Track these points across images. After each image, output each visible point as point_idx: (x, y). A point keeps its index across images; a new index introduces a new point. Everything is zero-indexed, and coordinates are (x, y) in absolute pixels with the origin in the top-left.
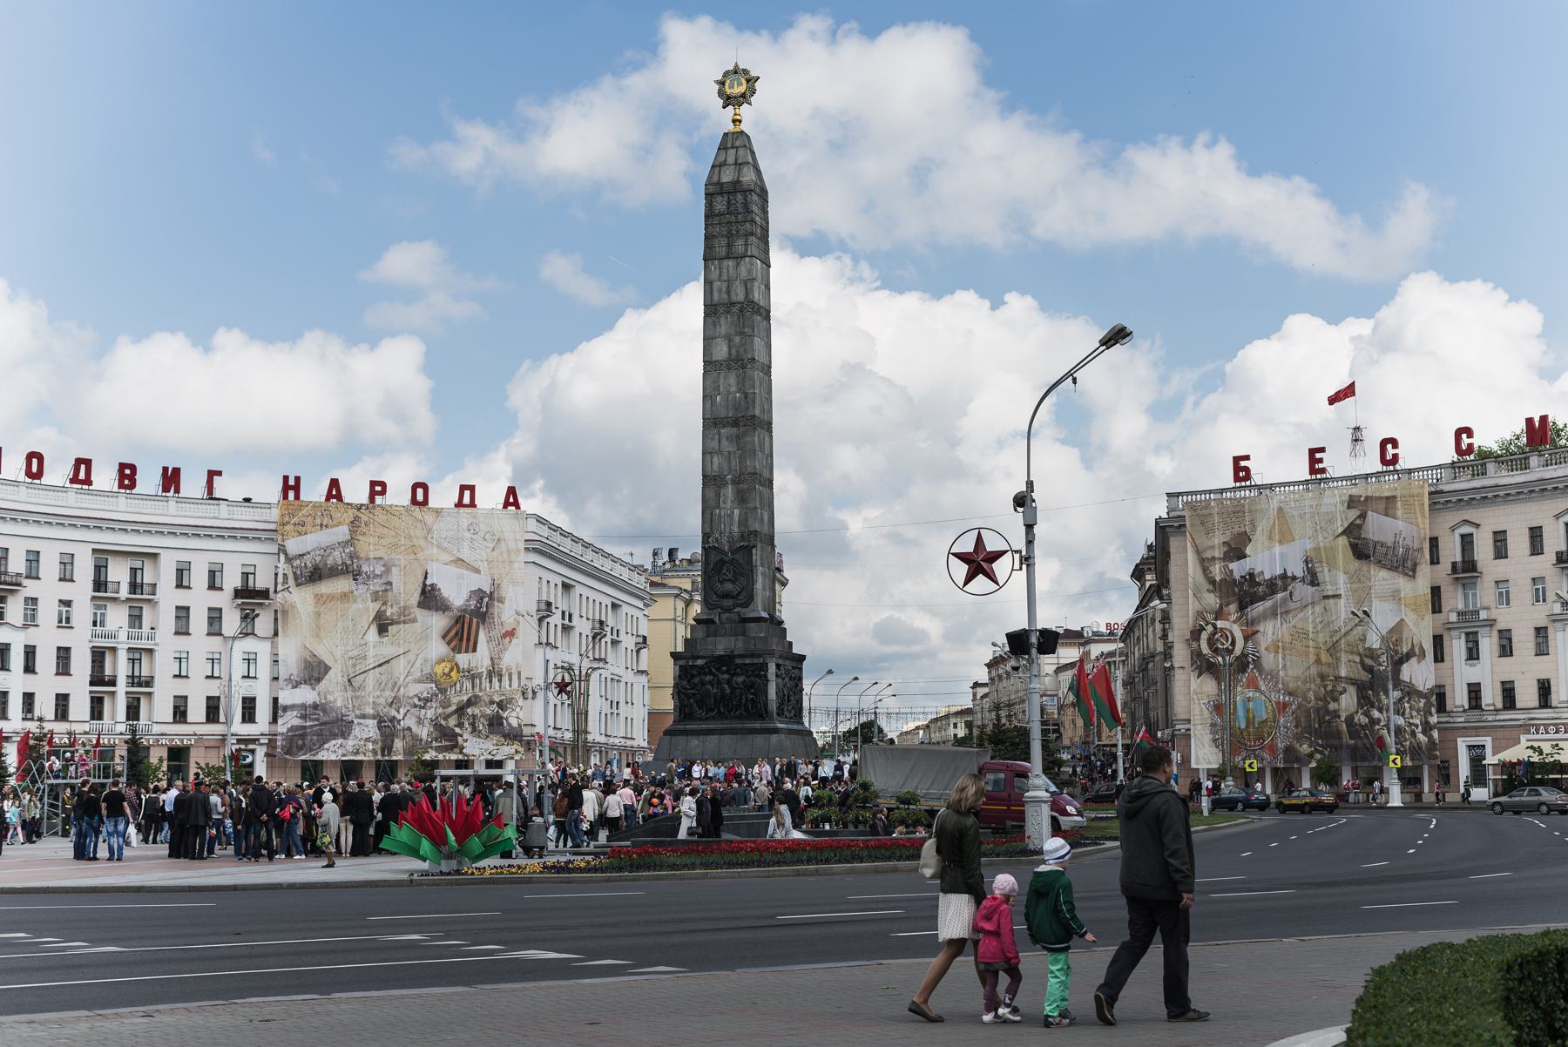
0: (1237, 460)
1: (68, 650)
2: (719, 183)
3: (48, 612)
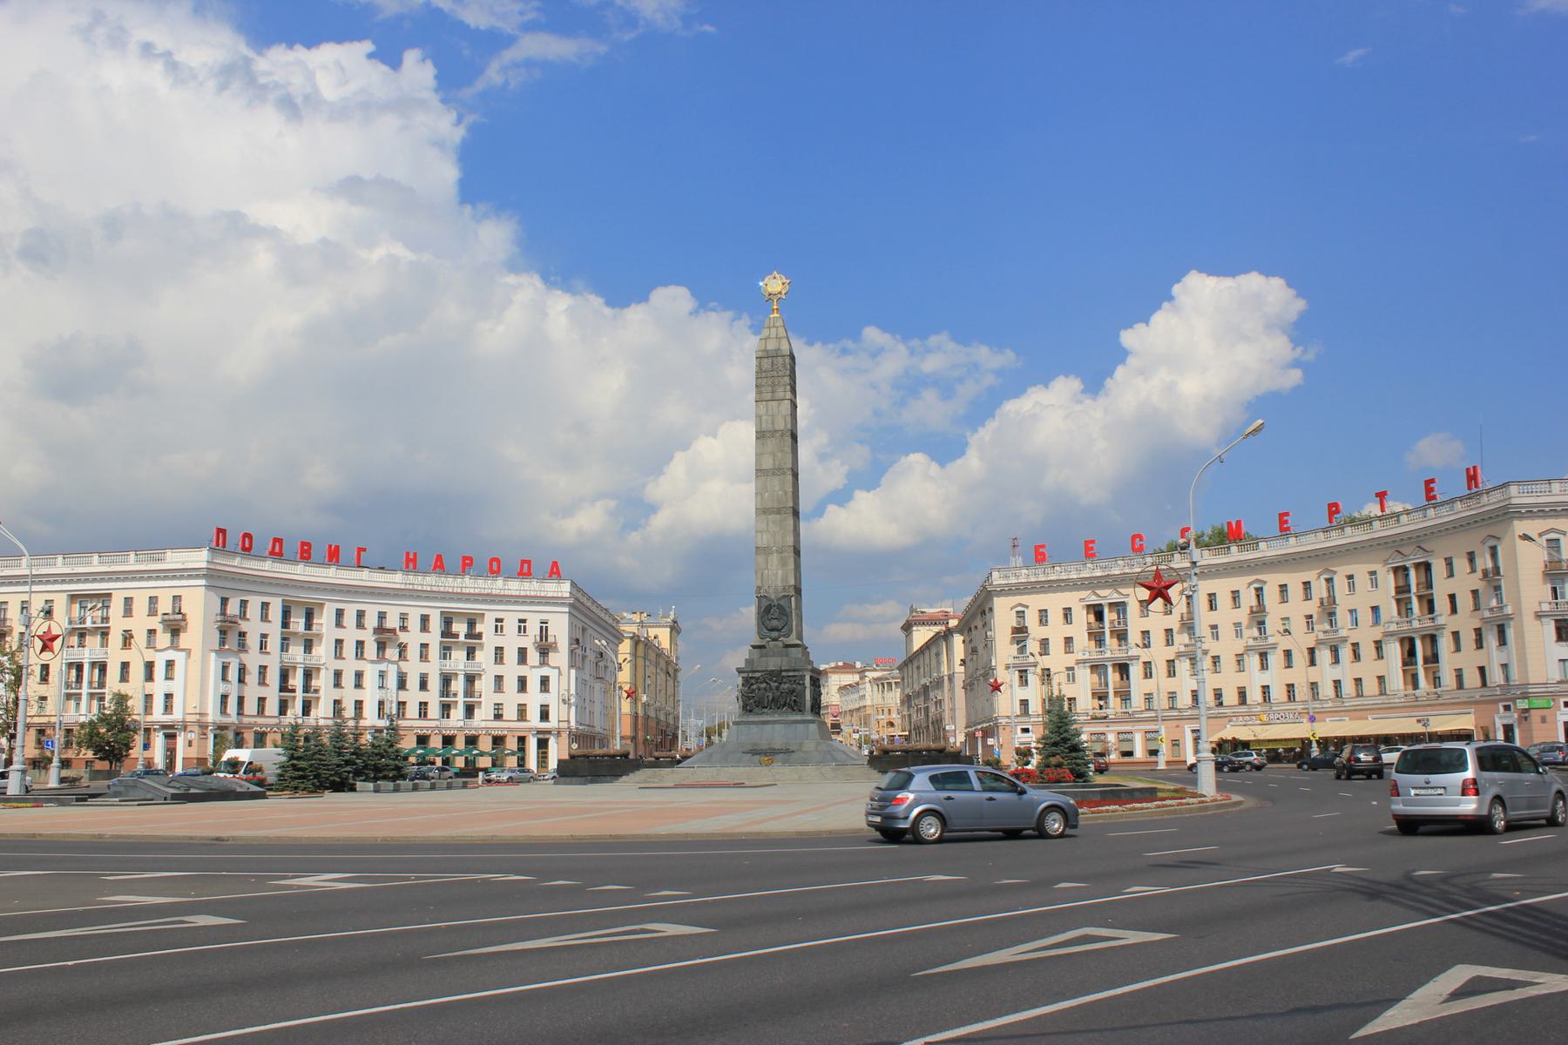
0: (1037, 548)
1: (265, 667)
2: (766, 351)
3: (413, 652)
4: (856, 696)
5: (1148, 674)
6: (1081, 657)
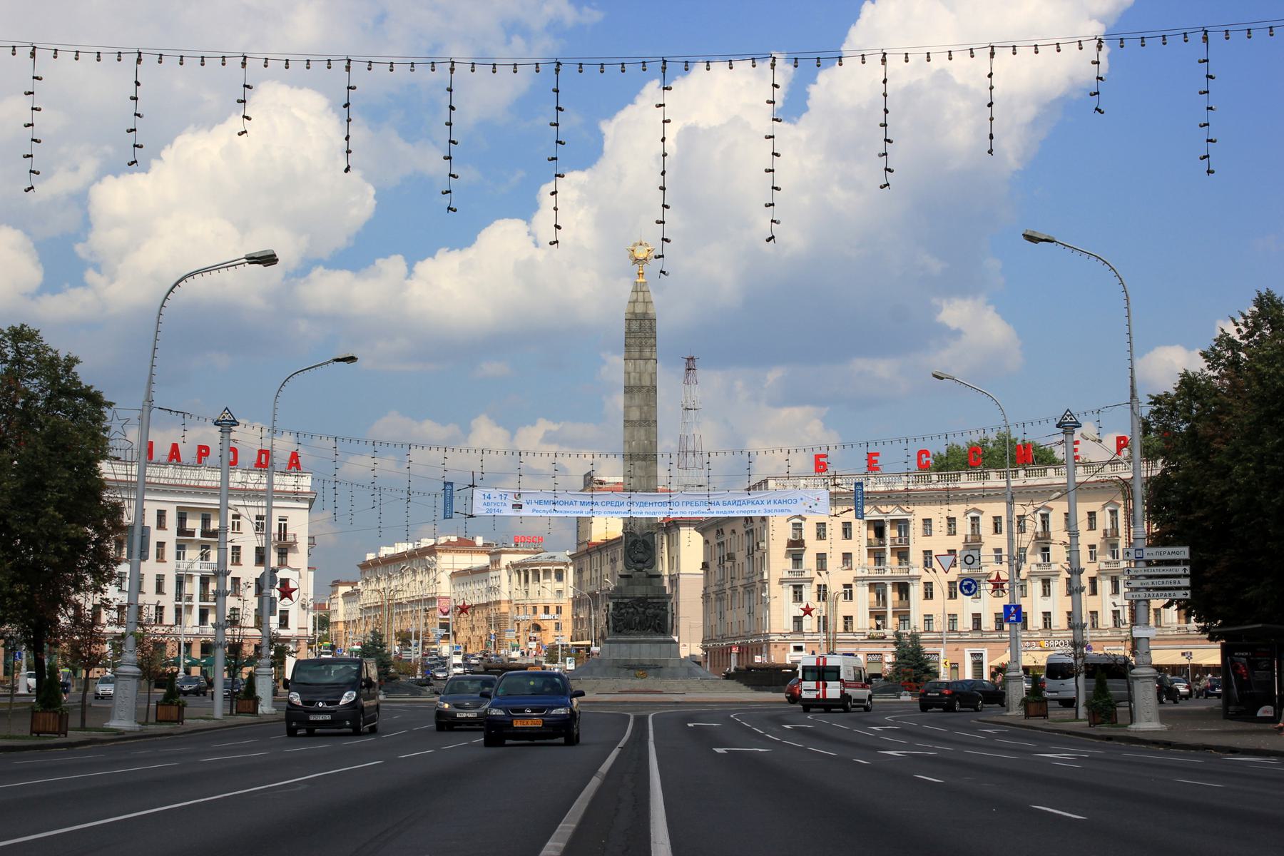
1: (926, 597)
2: (634, 313)
4: (483, 586)
5: (928, 595)
6: (859, 574)
